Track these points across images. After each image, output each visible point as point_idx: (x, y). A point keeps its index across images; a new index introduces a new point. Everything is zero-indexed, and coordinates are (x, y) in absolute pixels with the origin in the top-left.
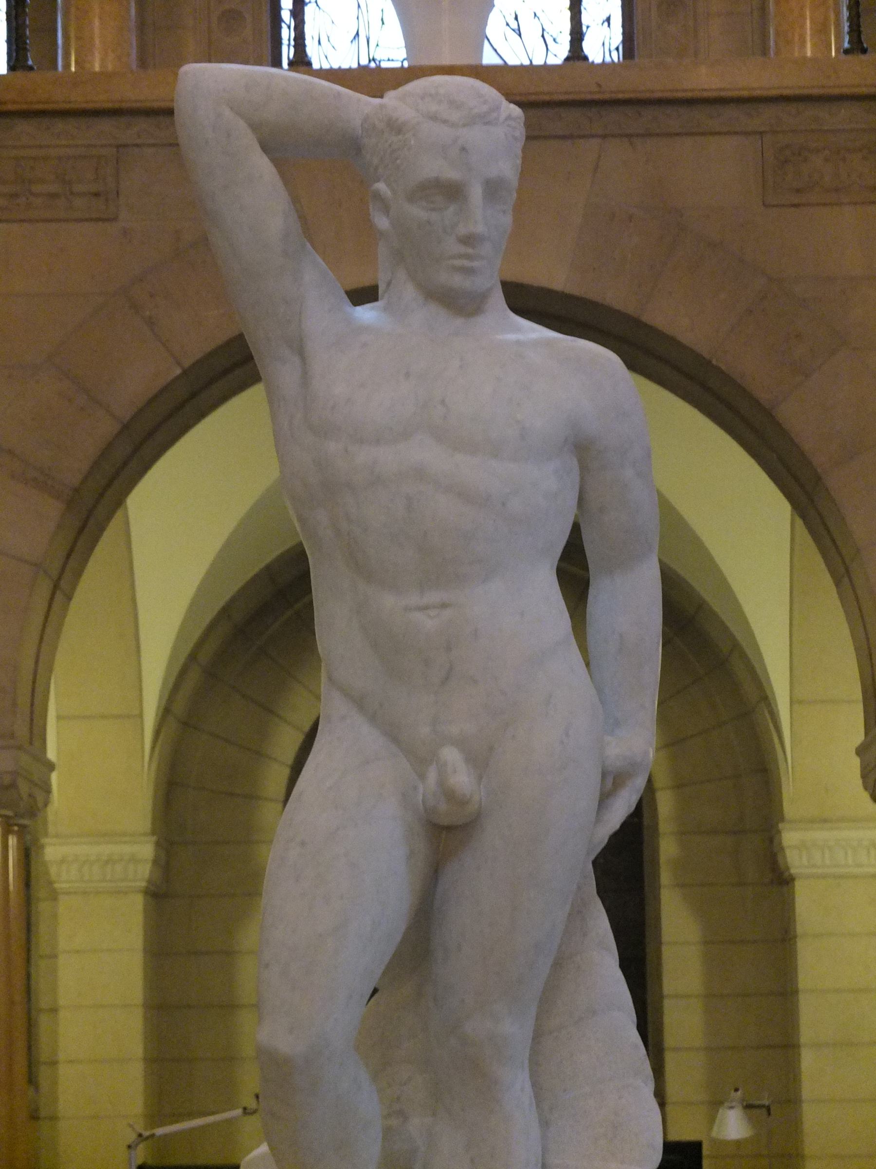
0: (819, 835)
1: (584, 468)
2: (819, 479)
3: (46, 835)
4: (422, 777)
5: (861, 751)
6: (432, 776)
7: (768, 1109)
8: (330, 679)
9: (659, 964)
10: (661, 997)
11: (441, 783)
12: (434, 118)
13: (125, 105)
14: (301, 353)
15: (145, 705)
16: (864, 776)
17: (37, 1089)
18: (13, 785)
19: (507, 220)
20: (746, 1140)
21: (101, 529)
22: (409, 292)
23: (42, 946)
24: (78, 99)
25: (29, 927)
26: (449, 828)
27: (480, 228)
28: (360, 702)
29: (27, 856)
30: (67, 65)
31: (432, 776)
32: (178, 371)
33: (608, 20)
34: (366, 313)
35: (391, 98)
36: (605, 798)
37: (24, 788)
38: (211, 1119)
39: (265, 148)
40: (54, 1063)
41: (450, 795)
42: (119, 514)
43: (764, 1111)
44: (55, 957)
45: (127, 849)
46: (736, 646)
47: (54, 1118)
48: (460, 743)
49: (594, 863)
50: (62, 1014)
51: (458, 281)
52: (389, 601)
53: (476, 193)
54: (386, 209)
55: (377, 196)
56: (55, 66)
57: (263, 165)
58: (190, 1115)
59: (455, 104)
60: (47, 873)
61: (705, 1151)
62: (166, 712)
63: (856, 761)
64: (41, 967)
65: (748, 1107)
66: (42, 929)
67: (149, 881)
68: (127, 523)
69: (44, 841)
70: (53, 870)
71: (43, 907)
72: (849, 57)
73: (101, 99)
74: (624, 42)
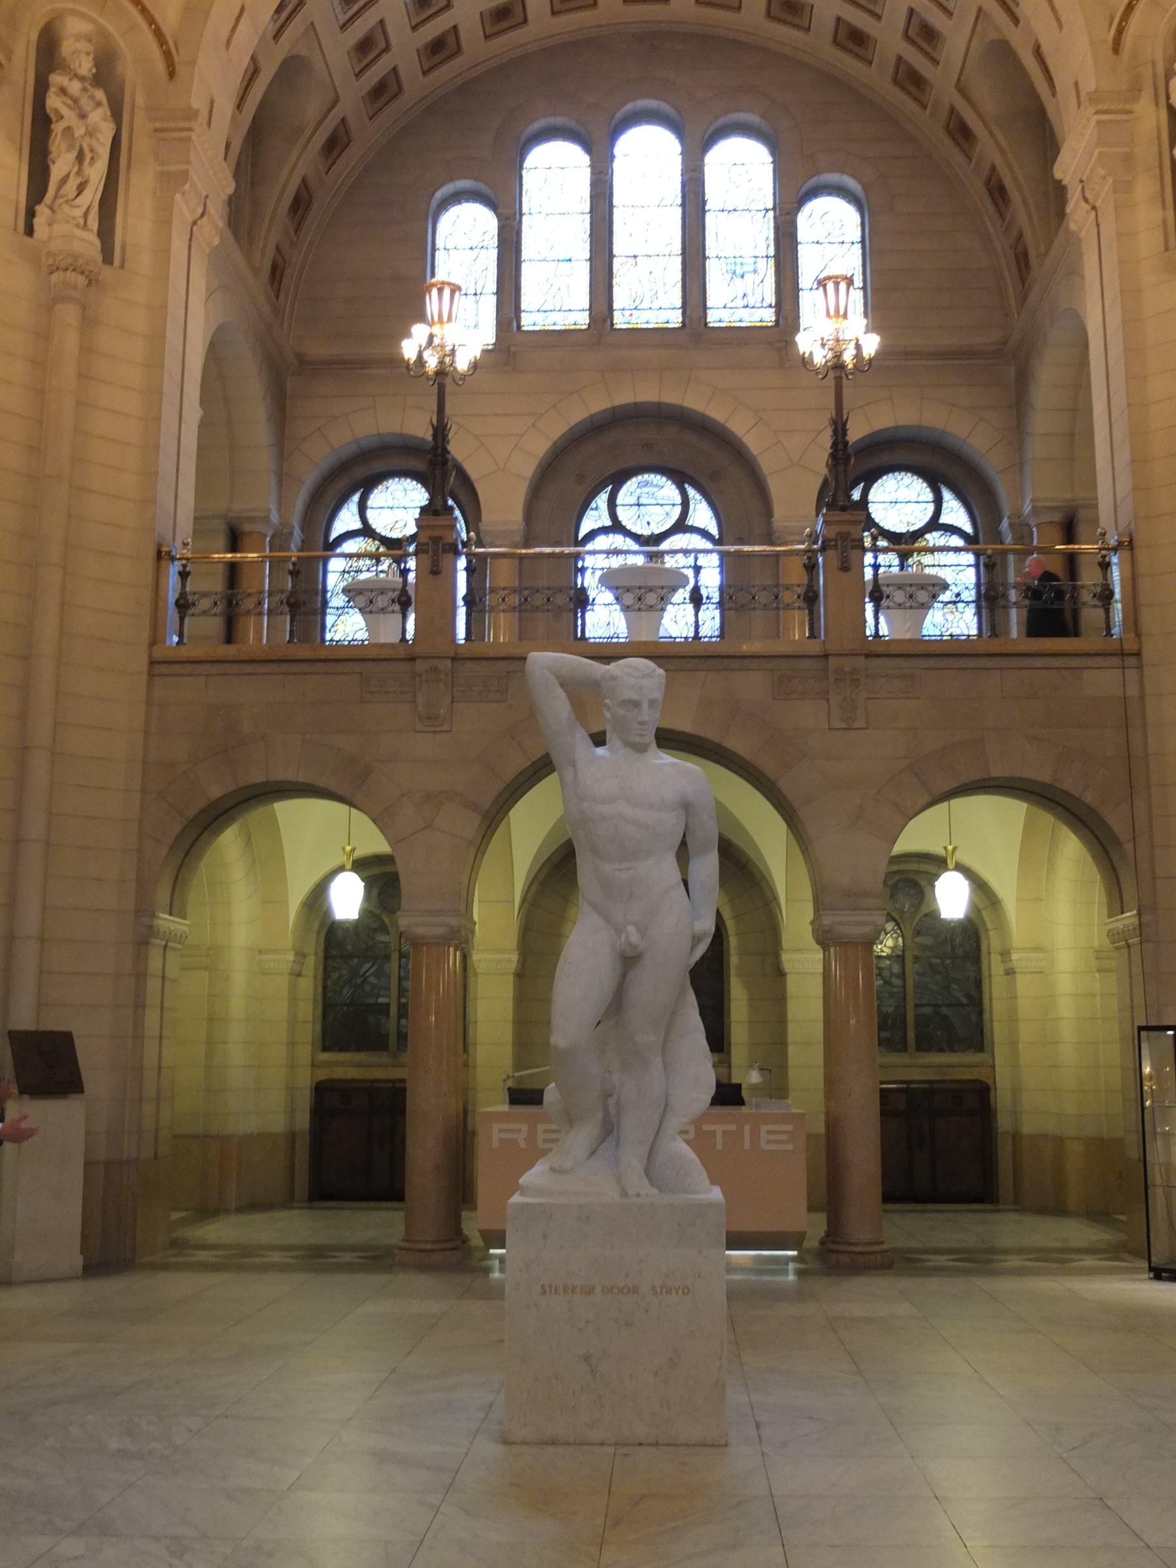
0: (794, 956)
1: (688, 815)
2: (795, 811)
3: (473, 949)
4: (620, 938)
5: (812, 923)
6: (623, 938)
7: (770, 1071)
8: (582, 897)
9: (729, 1008)
10: (730, 1022)
11: (627, 938)
12: (629, 675)
13: (510, 656)
14: (574, 767)
15: (515, 894)
16: (813, 933)
17: (468, 1055)
18: (459, 931)
19: (658, 715)
20: (761, 1083)
21: (497, 826)
22: (618, 743)
23: (471, 995)
24: (491, 653)
25: (465, 986)
26: (631, 958)
27: (647, 718)
28: (593, 906)
29: (465, 958)
30: (489, 639)
31: (623, 938)
32: (530, 763)
33: (713, 618)
34: (601, 751)
35: (613, 667)
36: (693, 948)
37: (463, 933)
38: (533, 1071)
39: (562, 685)
40: (475, 1044)
41: (631, 945)
42: (506, 819)
43: (768, 1072)
44: (477, 1000)
45: (506, 956)
46: (763, 877)
47: (475, 1067)
48: (635, 924)
49: (690, 972)
50: (478, 1023)
51: (638, 739)
52: (607, 867)
53: (645, 705)
54: (609, 709)
55: (605, 705)
56: (484, 640)
57: (560, 693)
58: (531, 1068)
59: (636, 669)
60: (474, 966)
61: (743, 1086)
62: (524, 900)
63: (810, 927)
64: (470, 1005)
65: (761, 1069)
66: (471, 987)
67: (516, 970)
68: (509, 820)
69: (472, 952)
70: (476, 964)
71: (471, 979)
72: (809, 640)
73: (502, 654)
74: (720, 627)
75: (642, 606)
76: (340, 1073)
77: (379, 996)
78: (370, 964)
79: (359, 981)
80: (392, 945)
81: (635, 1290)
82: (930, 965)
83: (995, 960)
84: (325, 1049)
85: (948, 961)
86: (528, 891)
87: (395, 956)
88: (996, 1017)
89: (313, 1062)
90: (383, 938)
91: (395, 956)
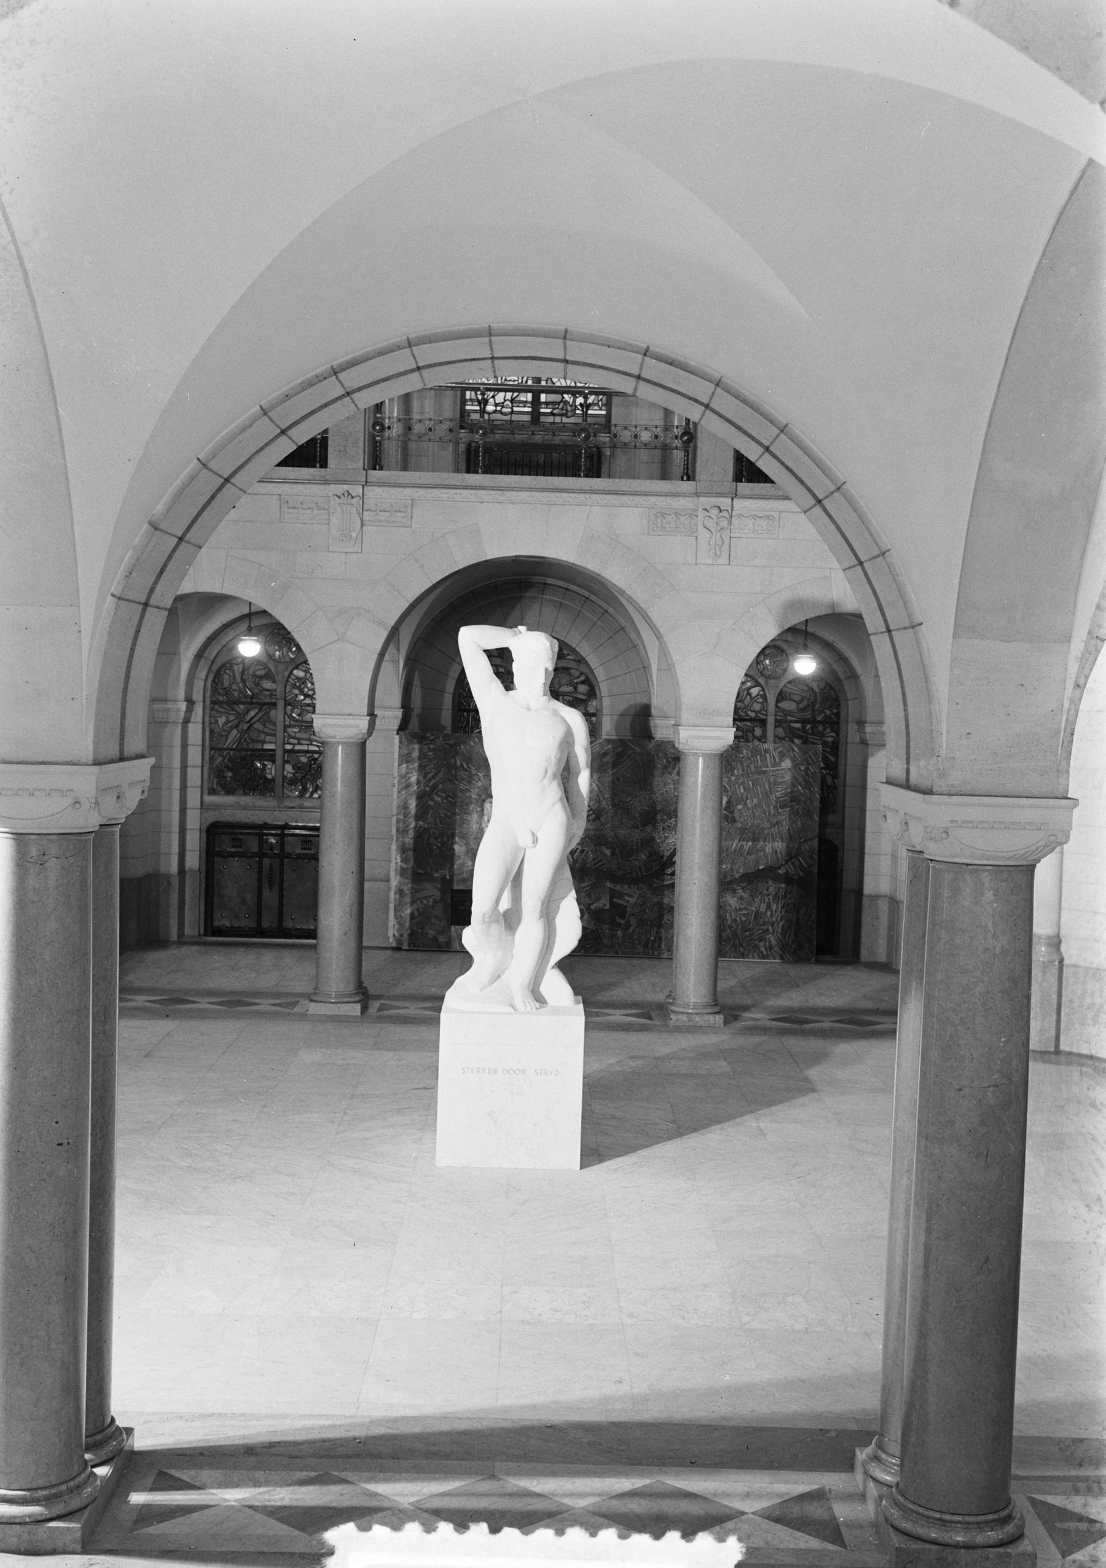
75: (654, 429)
76: (228, 816)
77: (264, 742)
78: (257, 710)
79: (245, 726)
80: (278, 693)
81: (524, 1072)
82: (791, 729)
83: (852, 728)
84: (212, 792)
85: (809, 726)
86: (412, 651)
87: (281, 704)
88: (849, 782)
89: (202, 804)
90: (267, 685)
91: (281, 704)
